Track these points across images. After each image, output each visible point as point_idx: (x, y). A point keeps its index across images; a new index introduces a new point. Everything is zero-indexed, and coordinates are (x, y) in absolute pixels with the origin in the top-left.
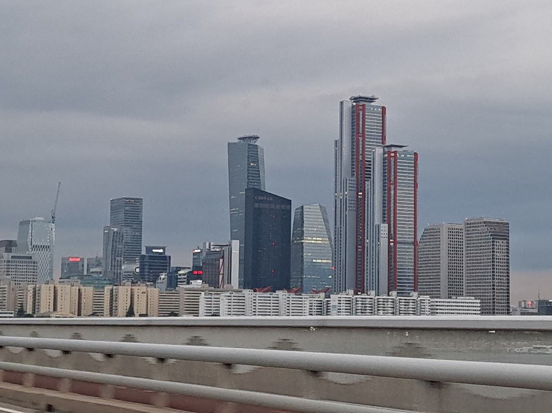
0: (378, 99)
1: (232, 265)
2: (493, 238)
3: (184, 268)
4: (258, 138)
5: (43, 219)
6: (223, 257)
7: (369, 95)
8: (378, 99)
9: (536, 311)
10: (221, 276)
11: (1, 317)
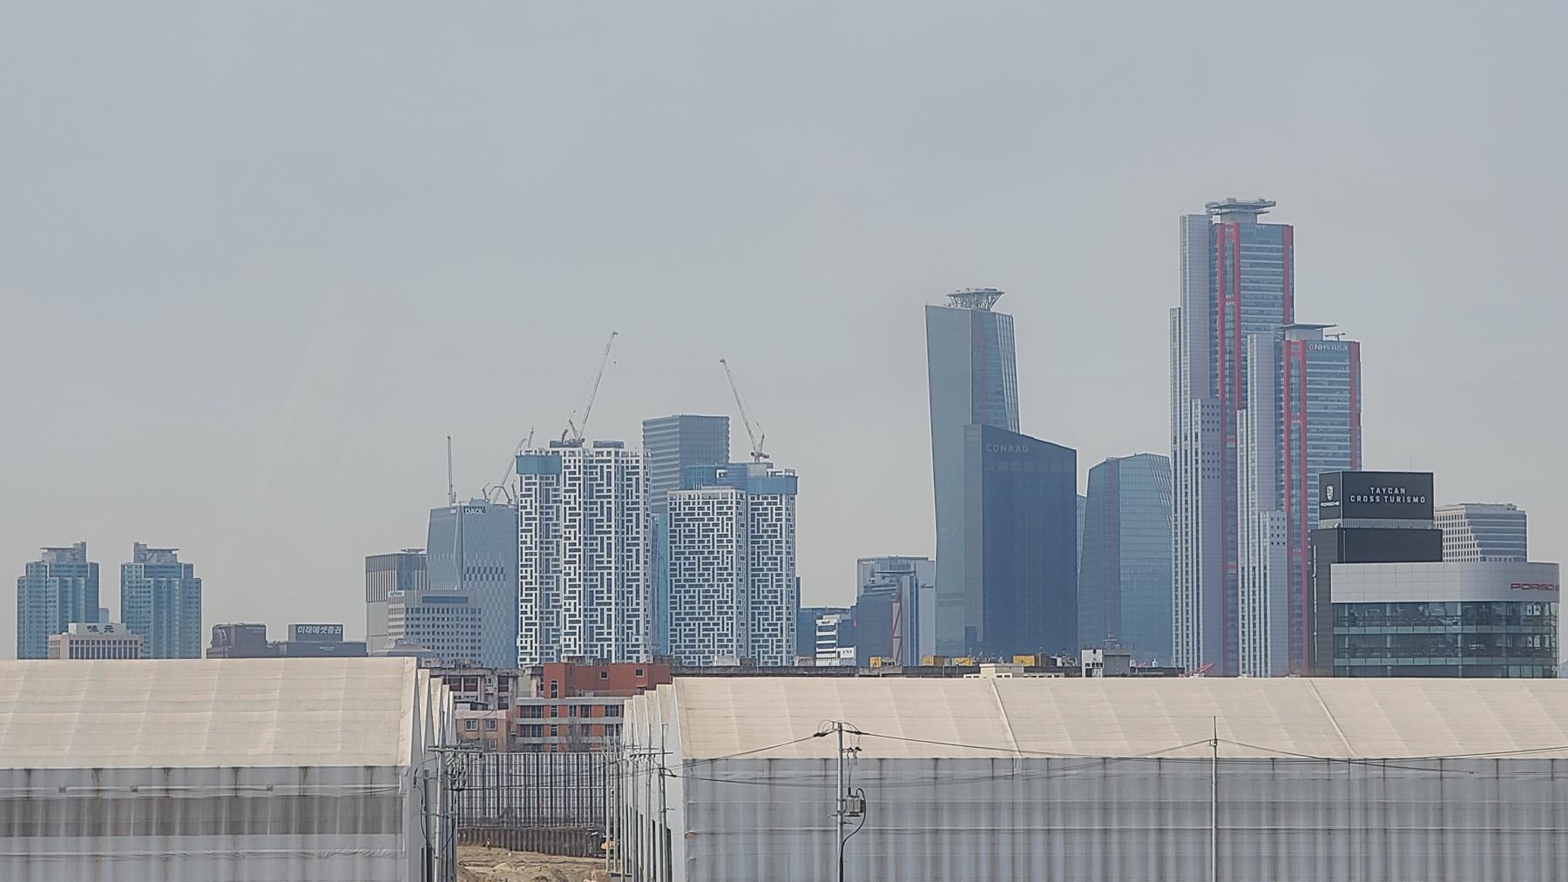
0: (1274, 204)
1: (920, 622)
2: (1483, 552)
3: (832, 611)
4: (1000, 293)
5: (978, 640)
6: (900, 599)
7: (1251, 198)
8: (1274, 204)
9: (1245, 410)
10: (896, 642)
11: (1386, 878)
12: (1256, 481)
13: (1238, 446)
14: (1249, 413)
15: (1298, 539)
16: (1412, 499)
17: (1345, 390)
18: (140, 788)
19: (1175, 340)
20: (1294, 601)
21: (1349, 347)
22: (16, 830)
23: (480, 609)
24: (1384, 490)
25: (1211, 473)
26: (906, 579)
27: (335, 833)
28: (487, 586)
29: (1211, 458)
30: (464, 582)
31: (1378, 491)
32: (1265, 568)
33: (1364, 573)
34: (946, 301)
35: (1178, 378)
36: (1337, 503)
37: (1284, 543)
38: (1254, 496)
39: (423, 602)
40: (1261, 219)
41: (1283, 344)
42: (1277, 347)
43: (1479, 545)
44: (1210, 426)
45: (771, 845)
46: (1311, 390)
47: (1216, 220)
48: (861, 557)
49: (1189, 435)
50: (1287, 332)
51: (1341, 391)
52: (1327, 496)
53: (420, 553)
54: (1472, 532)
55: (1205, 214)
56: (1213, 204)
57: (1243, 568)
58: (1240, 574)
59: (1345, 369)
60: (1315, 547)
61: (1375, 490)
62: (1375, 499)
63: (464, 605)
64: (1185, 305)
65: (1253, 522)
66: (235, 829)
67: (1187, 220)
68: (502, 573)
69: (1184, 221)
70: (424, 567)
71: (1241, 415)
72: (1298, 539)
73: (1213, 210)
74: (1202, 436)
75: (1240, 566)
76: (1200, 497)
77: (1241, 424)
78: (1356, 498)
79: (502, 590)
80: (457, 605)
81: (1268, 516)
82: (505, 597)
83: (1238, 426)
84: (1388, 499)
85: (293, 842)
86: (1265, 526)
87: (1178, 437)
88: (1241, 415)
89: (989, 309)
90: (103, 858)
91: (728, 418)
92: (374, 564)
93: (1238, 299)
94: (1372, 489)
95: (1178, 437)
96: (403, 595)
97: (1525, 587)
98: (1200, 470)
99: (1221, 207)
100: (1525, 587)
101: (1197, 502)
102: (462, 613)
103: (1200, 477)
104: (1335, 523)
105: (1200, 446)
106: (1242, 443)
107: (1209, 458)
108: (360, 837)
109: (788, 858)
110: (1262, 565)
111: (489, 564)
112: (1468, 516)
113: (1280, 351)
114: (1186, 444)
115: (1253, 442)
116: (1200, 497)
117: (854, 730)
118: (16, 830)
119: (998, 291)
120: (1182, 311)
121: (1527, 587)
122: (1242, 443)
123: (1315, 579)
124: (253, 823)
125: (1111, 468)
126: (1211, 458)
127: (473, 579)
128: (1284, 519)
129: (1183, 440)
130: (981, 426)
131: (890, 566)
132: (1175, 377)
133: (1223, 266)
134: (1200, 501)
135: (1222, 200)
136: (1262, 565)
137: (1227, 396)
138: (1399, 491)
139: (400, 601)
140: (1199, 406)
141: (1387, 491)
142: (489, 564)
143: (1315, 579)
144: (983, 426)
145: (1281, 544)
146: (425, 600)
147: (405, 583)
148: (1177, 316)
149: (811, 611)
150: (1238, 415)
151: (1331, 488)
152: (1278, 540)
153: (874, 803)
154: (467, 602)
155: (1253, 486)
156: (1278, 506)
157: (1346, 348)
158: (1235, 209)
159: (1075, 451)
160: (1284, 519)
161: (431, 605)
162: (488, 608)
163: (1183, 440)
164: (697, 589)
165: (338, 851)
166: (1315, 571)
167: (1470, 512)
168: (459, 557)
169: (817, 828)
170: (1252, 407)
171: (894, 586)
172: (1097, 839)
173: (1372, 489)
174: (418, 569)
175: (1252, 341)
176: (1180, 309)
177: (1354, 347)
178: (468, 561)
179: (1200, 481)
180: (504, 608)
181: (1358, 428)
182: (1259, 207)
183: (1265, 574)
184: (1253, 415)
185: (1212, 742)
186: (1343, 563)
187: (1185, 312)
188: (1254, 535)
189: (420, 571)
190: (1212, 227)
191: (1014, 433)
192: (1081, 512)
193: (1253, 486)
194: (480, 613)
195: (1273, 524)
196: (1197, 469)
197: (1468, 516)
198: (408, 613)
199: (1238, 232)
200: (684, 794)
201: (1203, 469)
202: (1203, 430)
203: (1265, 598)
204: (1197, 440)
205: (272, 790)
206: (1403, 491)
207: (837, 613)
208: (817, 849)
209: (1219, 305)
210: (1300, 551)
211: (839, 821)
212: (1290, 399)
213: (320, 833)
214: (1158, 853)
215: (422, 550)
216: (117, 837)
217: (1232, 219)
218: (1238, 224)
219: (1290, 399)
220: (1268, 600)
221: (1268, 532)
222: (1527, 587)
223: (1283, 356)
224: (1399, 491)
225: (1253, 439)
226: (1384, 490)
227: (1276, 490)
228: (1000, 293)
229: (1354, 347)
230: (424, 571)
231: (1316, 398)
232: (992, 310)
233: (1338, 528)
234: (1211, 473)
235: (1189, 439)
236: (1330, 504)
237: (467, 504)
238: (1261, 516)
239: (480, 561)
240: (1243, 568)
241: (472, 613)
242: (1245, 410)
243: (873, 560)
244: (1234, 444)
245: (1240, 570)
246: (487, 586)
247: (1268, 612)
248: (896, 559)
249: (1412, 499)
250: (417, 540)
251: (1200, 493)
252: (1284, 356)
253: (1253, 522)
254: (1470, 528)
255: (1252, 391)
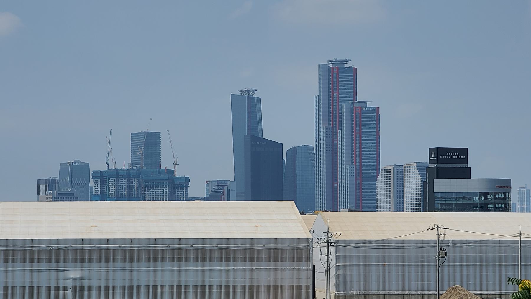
0: (350, 60)
4: (256, 90)
6: (224, 194)
7: (343, 59)
8: (350, 60)
12: (344, 154)
13: (338, 143)
14: (342, 131)
15: (359, 174)
16: (461, 157)
17: (374, 123)
18: (218, 245)
19: (316, 106)
20: (357, 195)
21: (376, 109)
22: (151, 260)
23: (78, 198)
24: (451, 154)
25: (329, 152)
26: (226, 187)
27: (286, 261)
28: (82, 190)
29: (329, 146)
30: (72, 188)
31: (449, 154)
32: (347, 184)
33: (451, 182)
34: (238, 93)
35: (318, 119)
36: (436, 158)
37: (354, 176)
38: (344, 159)
39: (58, 195)
40: (346, 66)
41: (354, 108)
42: (352, 109)
43: (421, 176)
44: (329, 136)
45: (365, 270)
46: (363, 124)
47: (331, 66)
48: (207, 180)
49: (321, 139)
50: (355, 104)
51: (373, 124)
52: (432, 156)
53: (56, 178)
54: (419, 172)
55: (327, 64)
56: (329, 60)
57: (340, 184)
58: (339, 186)
59: (374, 116)
60: (427, 173)
61: (448, 154)
62: (448, 157)
63: (72, 196)
64: (320, 94)
65: (343, 168)
66: (252, 260)
67: (321, 66)
68: (85, 185)
69: (320, 66)
70: (58, 183)
71: (339, 132)
72: (359, 174)
73: (329, 62)
74: (326, 139)
75: (339, 183)
76: (325, 160)
77: (339, 135)
78: (442, 157)
79: (85, 191)
80: (70, 196)
81: (348, 166)
82: (86, 194)
83: (338, 136)
84: (453, 157)
85: (272, 264)
86: (347, 170)
87: (318, 139)
88: (339, 132)
89: (253, 95)
90: (206, 270)
91: (160, 133)
92: (40, 182)
93: (338, 94)
94: (447, 153)
95: (318, 139)
96: (51, 193)
97: (500, 187)
98: (325, 151)
99: (332, 62)
100: (500, 187)
101: (324, 161)
102: (64, 199)
103: (325, 153)
104: (435, 165)
105: (325, 143)
106: (339, 141)
107: (328, 146)
108: (295, 263)
109: (371, 274)
110: (346, 183)
111: (80, 182)
112: (417, 167)
113: (353, 110)
114: (320, 142)
115: (343, 141)
116: (325, 160)
117: (443, 227)
118: (151, 260)
119: (256, 89)
120: (319, 96)
121: (501, 187)
122: (339, 141)
123: (428, 184)
124: (282, 258)
125: (293, 151)
126: (329, 146)
127: (79, 187)
128: (354, 167)
129: (319, 140)
130: (250, 135)
131: (217, 183)
132: (317, 119)
133: (333, 82)
134: (325, 161)
135: (333, 59)
136: (346, 183)
137: (334, 125)
138: (456, 154)
139: (50, 195)
140: (325, 129)
141: (452, 154)
142: (80, 182)
143: (428, 184)
144: (251, 135)
145: (353, 176)
146: (59, 194)
147: (51, 188)
148: (317, 98)
149: (190, 198)
150: (338, 132)
151: (433, 153)
152: (352, 174)
153: (382, 255)
154: (74, 195)
155: (343, 156)
156: (352, 163)
157: (375, 109)
158: (336, 62)
159: (282, 144)
160: (354, 167)
161: (61, 196)
162: (80, 197)
163: (319, 140)
164: (155, 191)
165: (288, 268)
166: (427, 182)
167: (418, 165)
168: (70, 180)
169: (381, 264)
170: (343, 129)
171: (222, 190)
172: (497, 268)
173: (447, 153)
174: (56, 184)
175: (343, 106)
176: (318, 96)
177: (378, 109)
178: (73, 181)
179: (325, 155)
180: (86, 197)
181: (379, 136)
182: (346, 61)
183: (347, 186)
184: (343, 132)
185: (519, 234)
186: (438, 179)
187: (320, 97)
188: (343, 173)
189: (56, 185)
190: (329, 68)
191: (261, 138)
192: (284, 165)
193: (343, 156)
194: (78, 199)
195: (350, 169)
196: (324, 150)
197: (417, 167)
198: (53, 199)
199: (338, 70)
200: (335, 251)
201: (326, 150)
202: (326, 137)
203: (347, 194)
204: (324, 141)
205: (264, 246)
206: (458, 154)
207: (200, 199)
208: (381, 271)
209: (332, 94)
210: (359, 178)
211: (437, 259)
212: (356, 127)
213: (281, 261)
214: (499, 273)
215: (57, 177)
216: (211, 263)
217: (336, 66)
218: (338, 67)
219: (356, 127)
220: (325, 196)
221: (348, 172)
222: (501, 187)
223: (354, 112)
224: (456, 154)
225: (343, 140)
226: (451, 154)
227: (351, 157)
228: (256, 90)
229: (378, 109)
230: (58, 185)
231: (365, 126)
232: (254, 96)
233: (436, 167)
234: (329, 152)
235: (321, 140)
236: (433, 159)
237: (73, 161)
238: (346, 166)
239: (81, 181)
240: (340, 184)
241: (75, 199)
242: (341, 130)
243: (211, 181)
244: (337, 142)
245: (339, 185)
246: (82, 190)
247: (348, 199)
248: (219, 181)
249: (461, 157)
250: (55, 174)
251: (325, 159)
252: (354, 112)
253: (343, 168)
254: (418, 170)
255: (343, 124)
